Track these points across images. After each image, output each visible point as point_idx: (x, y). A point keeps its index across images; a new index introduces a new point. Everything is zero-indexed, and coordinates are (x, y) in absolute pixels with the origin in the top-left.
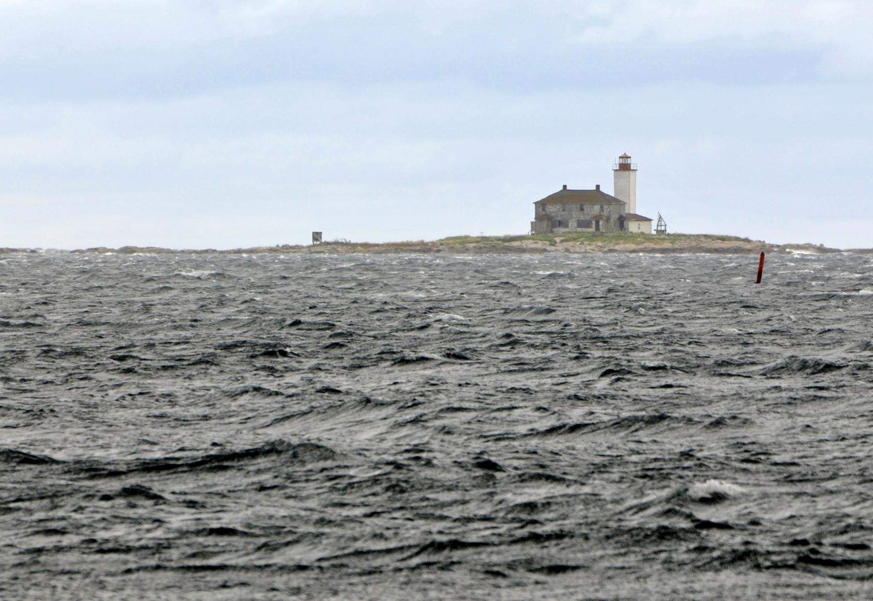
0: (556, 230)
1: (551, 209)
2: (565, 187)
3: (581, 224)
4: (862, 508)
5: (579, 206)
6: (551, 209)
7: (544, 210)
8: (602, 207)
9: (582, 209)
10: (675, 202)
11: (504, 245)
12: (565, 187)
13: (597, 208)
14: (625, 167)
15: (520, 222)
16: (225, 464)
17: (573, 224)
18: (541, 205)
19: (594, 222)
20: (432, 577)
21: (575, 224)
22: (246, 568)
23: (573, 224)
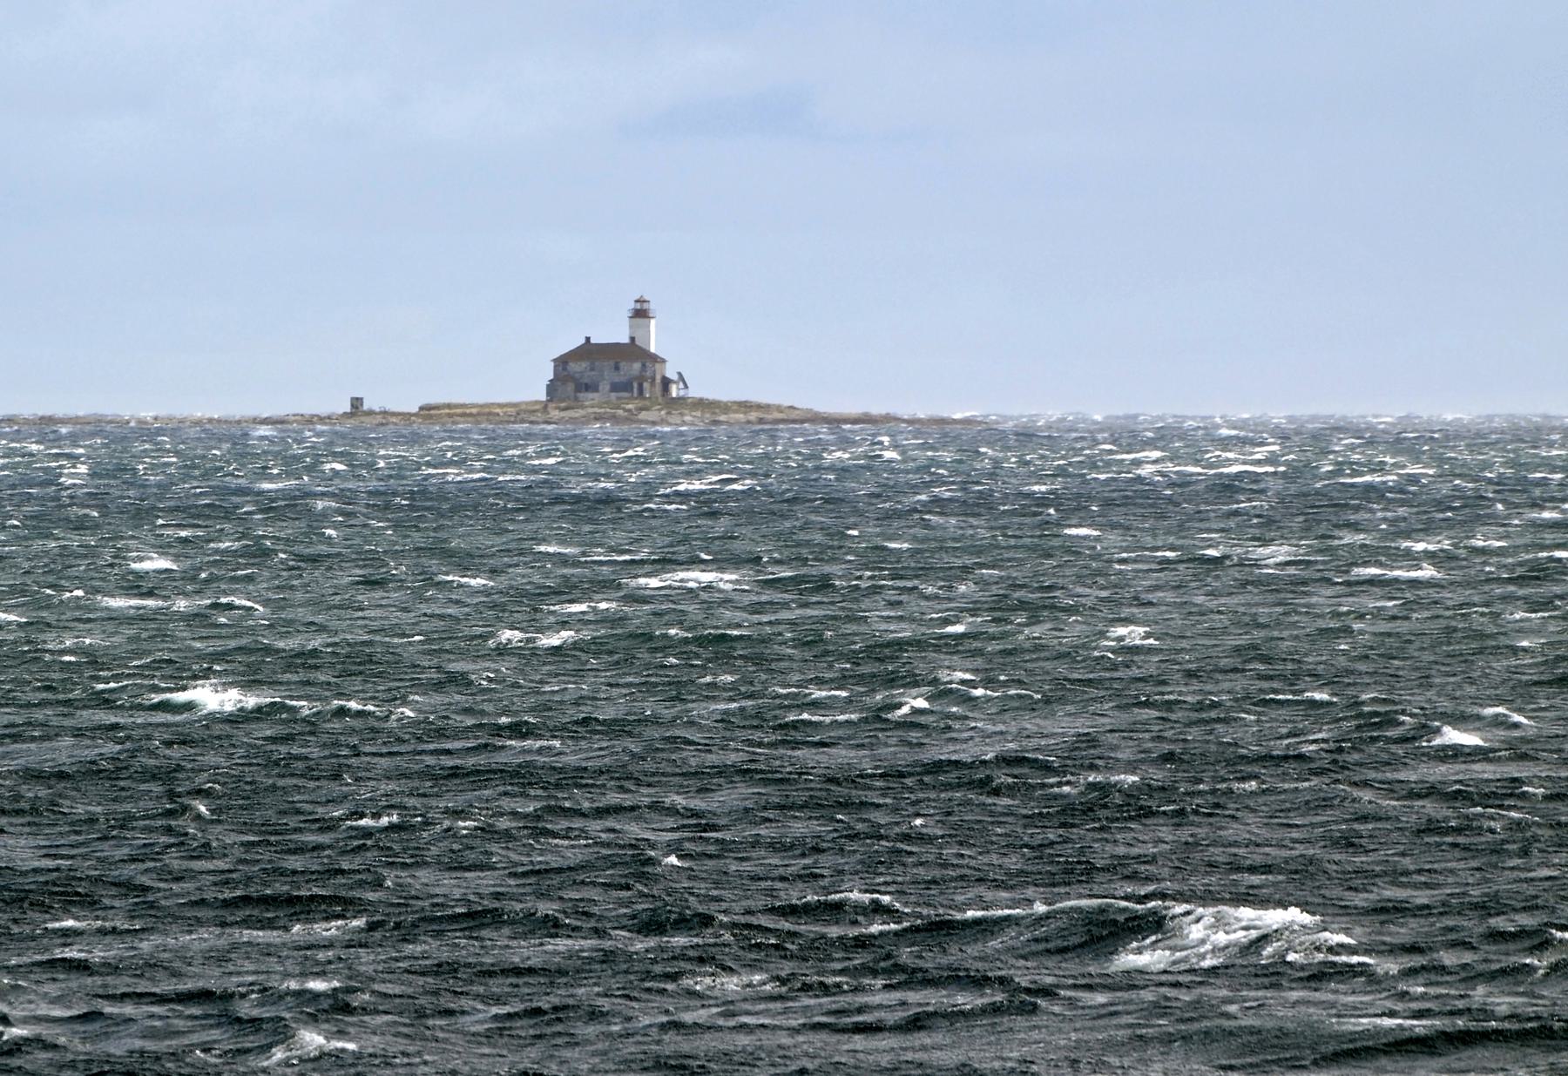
0: (581, 395)
1: (575, 367)
2: (588, 339)
3: (615, 388)
4: (692, 840)
5: (612, 363)
6: (575, 367)
7: (565, 369)
8: (644, 365)
9: (617, 368)
10: (708, 359)
11: (521, 412)
12: (588, 339)
13: (637, 366)
14: (641, 313)
15: (529, 383)
16: (1516, 1026)
17: (605, 387)
18: (562, 362)
19: (635, 385)
20: (812, 1002)
21: (608, 387)
22: (374, 754)
23: (605, 387)
